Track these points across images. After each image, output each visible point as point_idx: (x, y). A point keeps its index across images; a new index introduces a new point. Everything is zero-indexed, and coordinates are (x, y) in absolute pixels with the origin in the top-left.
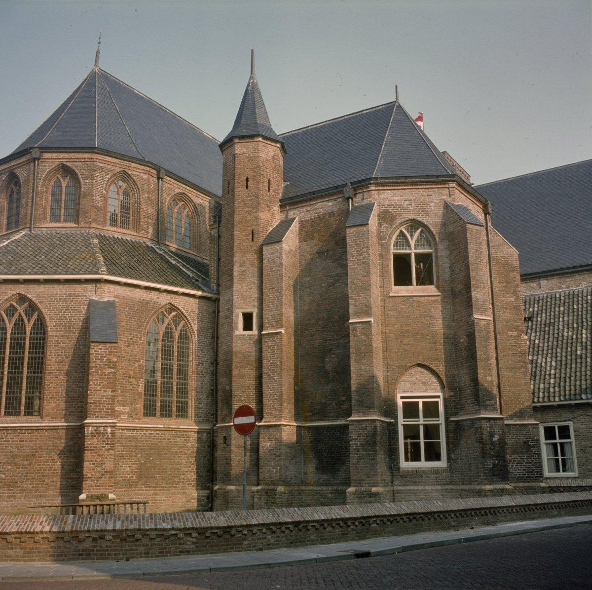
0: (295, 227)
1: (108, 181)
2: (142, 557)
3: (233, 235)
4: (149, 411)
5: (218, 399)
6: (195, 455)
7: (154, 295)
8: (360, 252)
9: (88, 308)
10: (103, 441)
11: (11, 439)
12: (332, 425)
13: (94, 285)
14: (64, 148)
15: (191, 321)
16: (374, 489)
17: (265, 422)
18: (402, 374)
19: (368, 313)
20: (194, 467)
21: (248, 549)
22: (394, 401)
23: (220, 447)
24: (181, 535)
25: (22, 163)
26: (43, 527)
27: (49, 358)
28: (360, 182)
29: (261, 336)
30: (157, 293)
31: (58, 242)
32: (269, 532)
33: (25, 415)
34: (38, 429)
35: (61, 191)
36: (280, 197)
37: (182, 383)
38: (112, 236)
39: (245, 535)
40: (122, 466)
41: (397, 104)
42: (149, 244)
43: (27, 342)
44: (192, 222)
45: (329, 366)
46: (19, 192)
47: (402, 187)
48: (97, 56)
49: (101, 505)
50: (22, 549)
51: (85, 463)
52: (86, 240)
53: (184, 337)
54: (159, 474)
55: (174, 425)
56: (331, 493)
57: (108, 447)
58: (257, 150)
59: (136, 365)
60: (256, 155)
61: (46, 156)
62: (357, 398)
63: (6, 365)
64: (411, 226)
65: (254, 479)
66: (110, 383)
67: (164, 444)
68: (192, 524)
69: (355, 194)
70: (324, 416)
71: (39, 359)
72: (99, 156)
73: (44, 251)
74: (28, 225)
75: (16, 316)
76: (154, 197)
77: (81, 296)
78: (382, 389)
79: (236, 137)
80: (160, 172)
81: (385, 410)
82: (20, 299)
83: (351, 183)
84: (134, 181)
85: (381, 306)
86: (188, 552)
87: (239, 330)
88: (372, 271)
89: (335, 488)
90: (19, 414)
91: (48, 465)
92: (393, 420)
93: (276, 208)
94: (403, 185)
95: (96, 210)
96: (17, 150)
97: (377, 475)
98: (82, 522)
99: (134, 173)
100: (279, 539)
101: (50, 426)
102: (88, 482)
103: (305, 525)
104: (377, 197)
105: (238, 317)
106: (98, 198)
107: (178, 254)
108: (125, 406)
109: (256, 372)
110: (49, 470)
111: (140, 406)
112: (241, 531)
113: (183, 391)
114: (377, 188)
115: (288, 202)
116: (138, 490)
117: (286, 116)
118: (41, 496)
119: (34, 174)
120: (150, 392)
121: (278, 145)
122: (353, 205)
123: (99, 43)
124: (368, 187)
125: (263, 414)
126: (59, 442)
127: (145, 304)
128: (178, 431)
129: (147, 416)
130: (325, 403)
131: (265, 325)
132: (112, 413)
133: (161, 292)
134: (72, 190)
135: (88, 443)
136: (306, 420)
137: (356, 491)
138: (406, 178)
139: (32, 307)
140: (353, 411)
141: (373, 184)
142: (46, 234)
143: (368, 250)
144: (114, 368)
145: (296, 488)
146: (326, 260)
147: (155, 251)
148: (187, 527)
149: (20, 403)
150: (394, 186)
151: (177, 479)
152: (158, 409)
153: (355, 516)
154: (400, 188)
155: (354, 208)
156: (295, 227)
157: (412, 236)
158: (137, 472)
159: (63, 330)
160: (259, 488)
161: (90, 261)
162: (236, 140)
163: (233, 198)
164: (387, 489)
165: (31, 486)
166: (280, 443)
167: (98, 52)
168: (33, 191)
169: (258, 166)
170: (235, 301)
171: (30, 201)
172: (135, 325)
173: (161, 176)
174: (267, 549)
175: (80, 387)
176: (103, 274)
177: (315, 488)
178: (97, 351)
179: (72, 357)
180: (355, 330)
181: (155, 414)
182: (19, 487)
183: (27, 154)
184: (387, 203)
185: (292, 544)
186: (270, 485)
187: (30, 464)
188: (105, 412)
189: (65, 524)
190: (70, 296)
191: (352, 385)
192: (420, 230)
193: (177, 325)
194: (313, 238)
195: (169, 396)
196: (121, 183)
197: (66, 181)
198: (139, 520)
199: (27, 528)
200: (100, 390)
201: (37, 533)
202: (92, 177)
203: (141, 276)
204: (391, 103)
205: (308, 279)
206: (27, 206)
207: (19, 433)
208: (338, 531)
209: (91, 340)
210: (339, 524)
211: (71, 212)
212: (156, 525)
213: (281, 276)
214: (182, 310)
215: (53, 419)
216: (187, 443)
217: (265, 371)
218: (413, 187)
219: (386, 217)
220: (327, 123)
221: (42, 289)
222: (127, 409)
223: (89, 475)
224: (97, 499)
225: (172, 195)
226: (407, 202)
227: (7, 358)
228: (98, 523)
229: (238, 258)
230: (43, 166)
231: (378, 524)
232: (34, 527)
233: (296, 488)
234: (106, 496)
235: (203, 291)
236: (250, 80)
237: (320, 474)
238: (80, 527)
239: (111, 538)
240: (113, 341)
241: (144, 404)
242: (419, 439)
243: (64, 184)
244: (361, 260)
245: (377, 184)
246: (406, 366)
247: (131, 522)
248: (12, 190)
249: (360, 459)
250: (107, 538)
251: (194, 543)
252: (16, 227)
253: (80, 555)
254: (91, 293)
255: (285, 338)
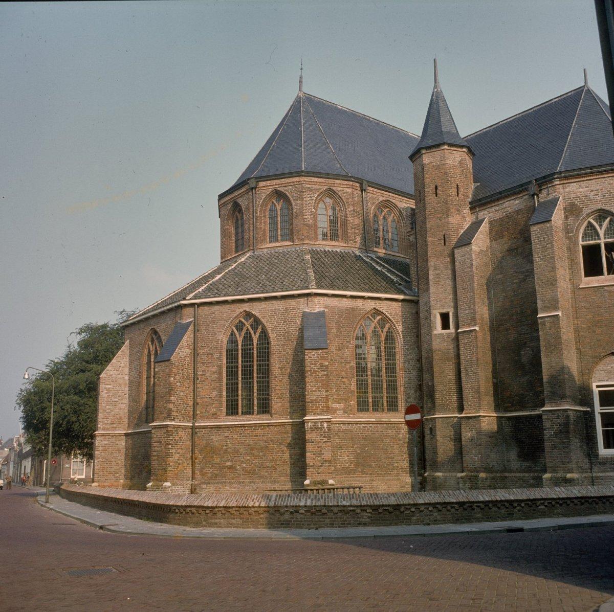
0: (484, 227)
1: (316, 200)
2: (328, 527)
3: (426, 241)
4: (363, 406)
5: (424, 396)
6: (406, 445)
7: (359, 303)
8: (545, 248)
9: (302, 319)
10: (321, 435)
11: (248, 434)
12: (531, 415)
13: (306, 299)
14: (276, 175)
15: (395, 323)
16: (569, 476)
17: (465, 414)
18: (597, 363)
19: (556, 308)
20: (406, 456)
21: (417, 523)
22: (590, 388)
23: (427, 437)
24: (358, 511)
25: (242, 193)
26: (255, 503)
27: (273, 364)
28: (544, 177)
29: (457, 334)
30: (362, 300)
31: (277, 261)
32: (435, 510)
33: (258, 414)
34: (269, 425)
35: (277, 214)
36: (470, 200)
37: (391, 380)
38: (323, 250)
39: (413, 512)
40: (341, 456)
41: (586, 88)
42: (357, 253)
43: (255, 352)
44: (398, 226)
45: (524, 359)
46: (242, 219)
47: (588, 178)
48: (301, 82)
49: (322, 489)
50: (241, 519)
51: (307, 454)
52: (300, 256)
53: (390, 338)
54: (374, 463)
55: (386, 418)
56: (533, 479)
57: (325, 439)
58: (443, 158)
59: (348, 367)
60: (443, 162)
61: (261, 184)
62: (549, 389)
63: (240, 372)
64: (599, 216)
65: (458, 467)
66: (323, 385)
67: (377, 435)
68: (367, 502)
69: (541, 190)
70: (523, 407)
71: (265, 366)
72: (306, 179)
73: (265, 270)
74: (251, 248)
75: (244, 331)
76: (359, 209)
77: (295, 309)
78: (576, 379)
79: (423, 148)
80: (363, 184)
81: (580, 399)
82: (246, 315)
83: (536, 180)
84: (339, 196)
85: (572, 298)
86: (365, 524)
87: (438, 329)
88: (558, 265)
89: (536, 474)
90: (253, 413)
91: (279, 456)
92: (589, 409)
93: (467, 211)
94: (588, 176)
95: (307, 228)
96: (238, 180)
97: (571, 462)
98: (282, 499)
99: (339, 189)
100: (446, 516)
101: (278, 423)
102: (310, 470)
103: (470, 505)
104: (562, 191)
105: (435, 317)
106: (308, 216)
107: (385, 259)
108: (340, 403)
109: (455, 367)
110: (280, 460)
111: (353, 403)
112: (409, 509)
113: (392, 387)
114: (562, 182)
115: (477, 204)
116: (356, 477)
117: (468, 122)
118: (275, 482)
119: (253, 201)
120: (362, 389)
121: (464, 150)
122: (538, 201)
123: (301, 69)
124: (553, 182)
125: (463, 406)
126: (286, 436)
127: (351, 312)
128: (389, 423)
129: (361, 411)
130: (522, 395)
131: (461, 324)
132: (328, 410)
133: (365, 299)
134: (286, 211)
135: (308, 436)
136: (506, 410)
137: (551, 478)
138: (591, 168)
139: (257, 322)
140: (546, 402)
141: (557, 178)
142: (266, 254)
143: (552, 246)
144: (326, 371)
145: (498, 475)
146: (516, 257)
147: (363, 259)
148: (363, 504)
149: (253, 404)
150: (579, 178)
151: (391, 467)
152: (371, 404)
153: (521, 498)
154: (586, 179)
155: (540, 204)
156: (484, 227)
157: (601, 226)
158: (354, 461)
159: (283, 340)
160: (463, 474)
161: (302, 277)
162: (424, 151)
163: (424, 206)
164: (586, 475)
165: (266, 473)
166: (479, 432)
167: (301, 78)
168: (253, 217)
169: (446, 174)
170: (433, 303)
171: (252, 226)
172: (344, 331)
173: (364, 188)
174: (434, 524)
175: (300, 388)
176: (312, 289)
177: (518, 475)
178: (311, 357)
179: (293, 363)
180: (543, 324)
181: (368, 409)
182: (257, 474)
183: (246, 184)
184: (573, 195)
185: (457, 521)
186: (472, 472)
187: (264, 455)
188: (321, 409)
189: (270, 501)
190: (286, 310)
191: (544, 377)
192: (609, 219)
193: (382, 328)
194: (502, 237)
195: (380, 392)
196: (328, 200)
197: (280, 204)
198: (325, 498)
199: (243, 504)
200: (315, 391)
201: (250, 507)
202: (302, 198)
203: (346, 286)
204: (580, 88)
205: (500, 276)
206: (249, 230)
207: (254, 429)
208: (503, 511)
209: (305, 348)
210: (504, 505)
211: (286, 231)
212: (338, 502)
213: (472, 276)
214: (387, 314)
215: (280, 416)
216: (399, 434)
217: (463, 366)
218: (599, 177)
219: (572, 210)
220: (517, 116)
221: (263, 305)
222: (342, 406)
223: (311, 464)
224: (319, 484)
225: (377, 203)
226: (593, 193)
227: (240, 366)
228: (294, 501)
229: (432, 263)
230: (260, 194)
231: (546, 506)
232: (248, 503)
233: (498, 475)
234: (326, 482)
235: (405, 294)
236: (434, 90)
237: (522, 461)
238: (281, 504)
239: (304, 512)
240: (324, 348)
241: (358, 401)
242: (603, 431)
243: (279, 207)
244: (545, 256)
245: (561, 178)
246: (600, 356)
247: (319, 500)
248: (237, 217)
249: (554, 447)
250: (301, 511)
251: (369, 517)
252: (242, 250)
253: (282, 524)
254: (305, 306)
255: (480, 335)
